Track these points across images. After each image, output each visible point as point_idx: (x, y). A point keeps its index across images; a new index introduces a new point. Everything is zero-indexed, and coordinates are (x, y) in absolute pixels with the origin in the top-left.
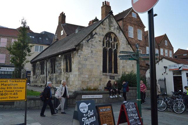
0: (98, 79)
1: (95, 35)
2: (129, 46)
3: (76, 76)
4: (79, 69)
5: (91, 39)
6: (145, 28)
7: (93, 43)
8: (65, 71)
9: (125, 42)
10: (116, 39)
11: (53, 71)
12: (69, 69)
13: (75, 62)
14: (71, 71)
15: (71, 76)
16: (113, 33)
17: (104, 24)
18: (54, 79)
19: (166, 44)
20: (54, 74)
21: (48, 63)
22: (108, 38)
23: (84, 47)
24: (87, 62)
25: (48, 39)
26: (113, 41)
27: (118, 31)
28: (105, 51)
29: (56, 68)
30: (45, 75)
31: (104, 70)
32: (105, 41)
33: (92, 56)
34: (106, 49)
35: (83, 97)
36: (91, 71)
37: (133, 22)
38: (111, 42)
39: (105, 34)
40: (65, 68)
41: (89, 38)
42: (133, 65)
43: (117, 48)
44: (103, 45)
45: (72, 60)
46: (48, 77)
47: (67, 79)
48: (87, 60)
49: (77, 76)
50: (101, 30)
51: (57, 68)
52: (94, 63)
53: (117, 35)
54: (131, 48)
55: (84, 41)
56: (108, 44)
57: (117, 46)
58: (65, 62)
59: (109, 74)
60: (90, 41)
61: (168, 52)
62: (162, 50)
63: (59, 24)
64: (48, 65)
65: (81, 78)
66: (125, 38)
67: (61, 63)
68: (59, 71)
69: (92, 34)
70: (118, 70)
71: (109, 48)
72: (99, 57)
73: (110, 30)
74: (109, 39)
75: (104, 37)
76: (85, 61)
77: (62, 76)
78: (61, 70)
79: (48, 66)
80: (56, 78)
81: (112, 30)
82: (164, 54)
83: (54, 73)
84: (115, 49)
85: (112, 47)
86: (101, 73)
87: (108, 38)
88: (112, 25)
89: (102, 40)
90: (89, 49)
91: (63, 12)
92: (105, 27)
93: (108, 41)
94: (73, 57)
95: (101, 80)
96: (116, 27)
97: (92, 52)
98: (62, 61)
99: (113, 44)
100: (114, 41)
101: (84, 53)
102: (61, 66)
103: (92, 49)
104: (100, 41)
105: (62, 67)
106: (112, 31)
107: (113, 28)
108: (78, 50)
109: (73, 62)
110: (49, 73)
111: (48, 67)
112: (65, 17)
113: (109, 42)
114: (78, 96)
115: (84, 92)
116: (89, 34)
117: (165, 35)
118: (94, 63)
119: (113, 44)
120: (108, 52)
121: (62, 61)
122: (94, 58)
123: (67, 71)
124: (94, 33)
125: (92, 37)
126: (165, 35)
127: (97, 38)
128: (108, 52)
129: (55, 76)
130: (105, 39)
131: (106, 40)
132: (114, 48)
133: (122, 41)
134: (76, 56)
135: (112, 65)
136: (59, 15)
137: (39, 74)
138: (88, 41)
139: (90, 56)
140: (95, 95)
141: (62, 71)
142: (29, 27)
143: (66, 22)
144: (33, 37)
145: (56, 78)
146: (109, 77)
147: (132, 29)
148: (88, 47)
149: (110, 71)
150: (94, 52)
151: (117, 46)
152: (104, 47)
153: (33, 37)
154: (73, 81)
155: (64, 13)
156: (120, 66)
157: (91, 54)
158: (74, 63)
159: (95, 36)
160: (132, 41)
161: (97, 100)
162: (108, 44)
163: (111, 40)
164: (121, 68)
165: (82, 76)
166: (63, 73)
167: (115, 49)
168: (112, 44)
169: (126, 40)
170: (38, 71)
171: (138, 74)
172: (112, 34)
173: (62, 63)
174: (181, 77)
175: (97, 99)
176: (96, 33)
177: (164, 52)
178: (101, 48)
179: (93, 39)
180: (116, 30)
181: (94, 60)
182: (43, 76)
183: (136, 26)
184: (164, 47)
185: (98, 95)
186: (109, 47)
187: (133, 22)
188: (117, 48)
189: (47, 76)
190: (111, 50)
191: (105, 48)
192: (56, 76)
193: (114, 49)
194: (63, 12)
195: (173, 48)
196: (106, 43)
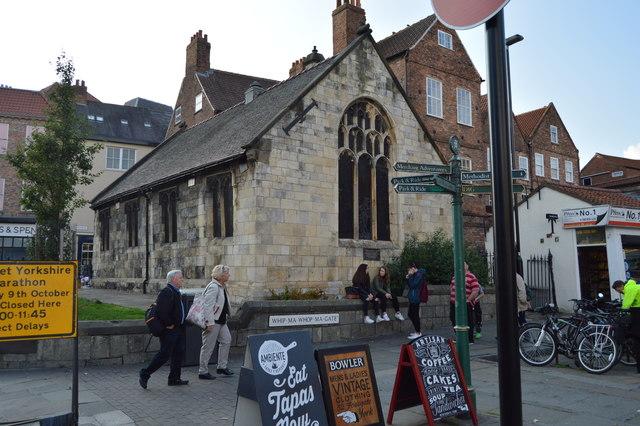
0: (323, 261)
1: (310, 107)
2: (429, 146)
3: (248, 249)
7: (306, 138)
8: (210, 232)
10: (383, 123)
11: (170, 234)
12: (222, 227)
13: (243, 202)
14: (230, 233)
16: (372, 101)
17: (341, 70)
19: (555, 139)
20: (174, 246)
21: (151, 208)
22: (355, 120)
23: (274, 151)
24: (286, 204)
25: (152, 123)
26: (373, 128)
27: (390, 93)
28: (345, 163)
29: (179, 225)
30: (143, 249)
31: (345, 230)
32: (347, 129)
33: (303, 182)
35: (274, 321)
36: (299, 233)
37: (440, 64)
38: (366, 132)
39: (345, 104)
40: (210, 222)
42: (441, 210)
43: (387, 153)
44: (341, 144)
46: (153, 255)
50: (332, 91)
53: (387, 107)
54: (435, 153)
55: (274, 131)
56: (358, 138)
57: (387, 146)
58: (210, 203)
60: (294, 128)
61: (562, 165)
62: (539, 159)
64: (151, 214)
65: (267, 258)
66: (413, 117)
68: (191, 235)
69: (301, 108)
70: (393, 228)
71: (360, 153)
73: (363, 91)
74: (360, 124)
76: (278, 201)
77: (202, 252)
78: (198, 230)
80: (180, 259)
81: (370, 90)
83: (175, 240)
84: (382, 155)
85: (369, 149)
86: (333, 239)
87: (355, 120)
88: (368, 74)
90: (293, 156)
91: (201, 31)
93: (355, 129)
94: (236, 187)
95: (332, 263)
96: (384, 80)
97: (301, 167)
99: (373, 139)
102: (196, 216)
103: (301, 157)
104: (328, 130)
105: (201, 221)
106: (371, 96)
107: (373, 83)
111: (151, 222)
112: (208, 47)
113: (360, 134)
114: (258, 320)
115: (277, 304)
116: (291, 107)
119: (373, 139)
123: (217, 233)
124: (307, 101)
125: (302, 115)
128: (356, 167)
131: (351, 127)
132: (377, 152)
136: (189, 42)
137: (122, 245)
138: (287, 130)
139: (294, 180)
140: (313, 313)
141: (201, 235)
142: (83, 82)
144: (100, 119)
145: (180, 259)
146: (360, 254)
149: (365, 232)
150: (309, 167)
151: (387, 146)
152: (342, 149)
153: (100, 119)
154: (237, 268)
155: (206, 36)
158: (242, 205)
159: (313, 111)
160: (438, 130)
163: (368, 127)
164: (401, 222)
165: (270, 250)
166: (203, 241)
167: (382, 155)
168: (369, 141)
169: (415, 123)
170: (118, 236)
172: (368, 107)
173: (201, 207)
174: (603, 250)
175: (320, 330)
176: (315, 104)
177: (547, 164)
178: (334, 155)
179: (304, 124)
180: (383, 91)
182: (136, 251)
184: (548, 149)
185: (323, 316)
186: (360, 149)
187: (440, 64)
189: (148, 254)
191: (346, 152)
193: (379, 157)
194: (201, 31)
196: (350, 134)
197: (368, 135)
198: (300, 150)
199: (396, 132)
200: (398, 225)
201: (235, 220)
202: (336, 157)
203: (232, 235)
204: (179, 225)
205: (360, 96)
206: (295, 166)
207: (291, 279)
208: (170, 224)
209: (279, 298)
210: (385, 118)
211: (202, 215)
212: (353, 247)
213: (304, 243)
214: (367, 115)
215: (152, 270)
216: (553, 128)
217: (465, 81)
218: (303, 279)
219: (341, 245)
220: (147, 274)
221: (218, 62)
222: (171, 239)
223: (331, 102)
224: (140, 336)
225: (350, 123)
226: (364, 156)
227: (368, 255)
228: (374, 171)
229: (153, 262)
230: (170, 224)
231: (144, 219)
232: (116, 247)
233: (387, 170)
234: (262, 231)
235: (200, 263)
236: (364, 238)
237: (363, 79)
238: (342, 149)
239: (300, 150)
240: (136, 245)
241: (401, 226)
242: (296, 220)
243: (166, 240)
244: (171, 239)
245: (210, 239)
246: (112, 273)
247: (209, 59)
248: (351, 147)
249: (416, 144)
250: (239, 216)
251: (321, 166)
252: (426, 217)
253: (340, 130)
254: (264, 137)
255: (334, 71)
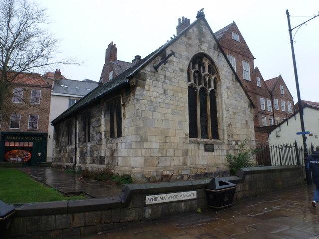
0: (180, 153)
1: (170, 56)
2: (238, 84)
3: (131, 146)
4: (138, 129)
5: (163, 65)
6: (254, 60)
7: (168, 74)
8: (108, 135)
9: (231, 75)
10: (213, 69)
11: (87, 137)
12: (115, 131)
13: (127, 115)
14: (119, 135)
15: (119, 145)
18: (89, 154)
19: (282, 92)
20: (89, 145)
21: (77, 123)
22: (197, 66)
23: (148, 81)
24: (156, 115)
26: (207, 72)
27: (216, 52)
28: (192, 89)
29: (91, 132)
30: (74, 147)
31: (193, 133)
32: (193, 71)
33: (167, 101)
34: (195, 88)
36: (164, 134)
38: (203, 74)
39: (191, 56)
40: (108, 129)
41: (159, 62)
42: (246, 121)
43: (215, 87)
44: (189, 80)
45: (122, 111)
46: (78, 150)
47: (113, 152)
48: (154, 110)
49: (133, 147)
51: (94, 130)
52: (170, 116)
53: (215, 60)
54: (241, 88)
55: (148, 68)
58: (108, 117)
59: (203, 140)
60: (160, 67)
61: (286, 105)
62: (276, 101)
63: (106, 62)
64: (78, 126)
65: (143, 151)
66: (229, 67)
67: (99, 120)
68: (97, 138)
70: (220, 132)
71: (200, 86)
72: (180, 104)
75: (189, 62)
76: (150, 113)
77: (103, 148)
78: (101, 134)
79: (78, 129)
80: (92, 152)
81: (205, 49)
82: (280, 108)
83: (89, 141)
85: (205, 84)
86: (186, 138)
87: (197, 66)
88: (203, 40)
89: (186, 68)
90: (160, 84)
91: (112, 42)
92: (190, 43)
94: (123, 105)
95: (186, 154)
97: (165, 92)
98: (103, 116)
99: (207, 78)
100: (210, 72)
101: (149, 94)
102: (100, 126)
103: (165, 85)
104: (182, 70)
105: (103, 129)
106: (206, 52)
108: (134, 87)
109: (124, 116)
110: (79, 141)
111: (78, 131)
112: (116, 50)
113: (200, 75)
115: (151, 186)
117: (280, 76)
118: (170, 116)
119: (207, 78)
120: (198, 94)
121: (103, 116)
122: (172, 106)
123: (112, 136)
124: (168, 52)
126: (280, 76)
127: (175, 64)
128: (198, 94)
129: (89, 148)
130: (192, 67)
132: (210, 87)
133: (223, 72)
134: (130, 102)
135: (206, 122)
136: (107, 47)
137: (64, 145)
138: (156, 68)
139: (161, 100)
141: (103, 137)
142: (59, 70)
143: (118, 59)
145: (92, 152)
146: (202, 147)
147: (234, 60)
148: (157, 80)
149: (205, 135)
150: (170, 93)
152: (190, 83)
154: (124, 158)
156: (223, 123)
157: (165, 97)
158: (127, 116)
159: (172, 58)
161: (183, 204)
162: (199, 77)
163: (204, 71)
164: (225, 128)
165: (146, 145)
166: (104, 141)
168: (205, 79)
170: (64, 140)
171: (46, 164)
173: (103, 121)
176: (173, 54)
177: (280, 104)
178: (185, 85)
179: (167, 65)
180: (212, 50)
181: (169, 111)
182: (70, 147)
183: (240, 56)
184: (280, 96)
185: (164, 195)
186: (200, 84)
188: (215, 87)
189: (76, 149)
190: (203, 90)
191: (192, 85)
192: (92, 147)
193: (211, 89)
194: (112, 42)
195: (292, 98)
196: (194, 74)
197: (204, 76)
198: (164, 81)
199: (221, 75)
200: (223, 129)
201: (122, 126)
202: (187, 87)
203: (205, 151)
204: (91, 132)
205: (200, 52)
206: (162, 91)
207: (160, 165)
208: (87, 131)
209: (155, 181)
210: (214, 67)
211: (104, 126)
212: (199, 143)
213: (168, 141)
214: (204, 64)
215: (78, 158)
216: (281, 87)
217: (246, 58)
218: (168, 164)
219: (191, 142)
220: (75, 160)
221: (120, 56)
222: (87, 141)
223: (183, 53)
224: (37, 217)
225: (194, 68)
226: (202, 88)
227: (207, 148)
228: (208, 97)
229: (78, 154)
230: (87, 131)
231: (74, 129)
232: (62, 145)
233: (216, 97)
234: (141, 133)
235: (103, 155)
236: (204, 138)
237: (201, 42)
238: (190, 83)
239: (164, 81)
240: (71, 144)
241: (225, 130)
242: (162, 126)
243: (85, 142)
244: (87, 141)
245: (107, 140)
246: (60, 160)
247: (116, 55)
248: (195, 81)
249: (231, 82)
250: (125, 123)
251: (178, 92)
252: (238, 125)
253: (188, 71)
254: (142, 71)
255: (184, 35)
